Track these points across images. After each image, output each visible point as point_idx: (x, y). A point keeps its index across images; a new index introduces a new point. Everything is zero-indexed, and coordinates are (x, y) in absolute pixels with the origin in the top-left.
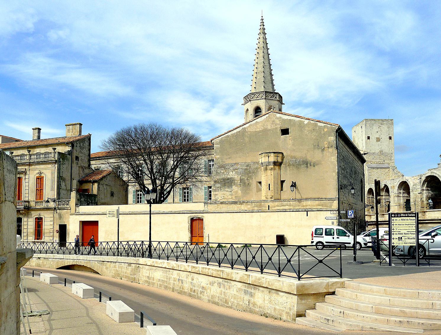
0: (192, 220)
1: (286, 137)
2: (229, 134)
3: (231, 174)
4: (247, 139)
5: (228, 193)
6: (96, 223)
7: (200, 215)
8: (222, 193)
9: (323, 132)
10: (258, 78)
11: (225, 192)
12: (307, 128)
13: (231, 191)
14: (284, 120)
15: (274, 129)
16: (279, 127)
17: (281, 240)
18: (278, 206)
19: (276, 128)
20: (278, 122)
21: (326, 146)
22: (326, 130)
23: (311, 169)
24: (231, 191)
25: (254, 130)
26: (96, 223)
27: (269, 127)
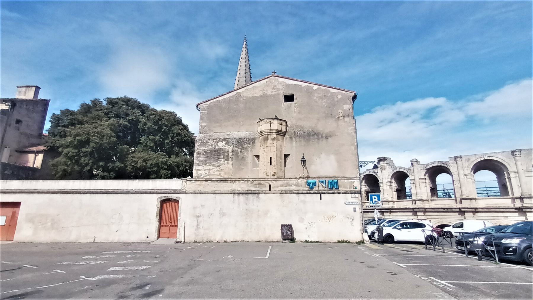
0: (164, 202)
1: (291, 104)
2: (221, 98)
3: (221, 145)
4: (241, 105)
5: (215, 169)
6: (177, 201)
7: (174, 196)
8: (208, 167)
9: (336, 99)
10: (240, 81)
11: (211, 167)
12: (316, 95)
13: (219, 166)
14: (288, 86)
15: (275, 95)
16: (283, 92)
17: (288, 233)
18: (282, 186)
19: (278, 94)
20: (280, 86)
21: (341, 115)
22: (339, 97)
23: (323, 142)
24: (219, 166)
25: (251, 96)
26: (17, 205)
27: (269, 93)
